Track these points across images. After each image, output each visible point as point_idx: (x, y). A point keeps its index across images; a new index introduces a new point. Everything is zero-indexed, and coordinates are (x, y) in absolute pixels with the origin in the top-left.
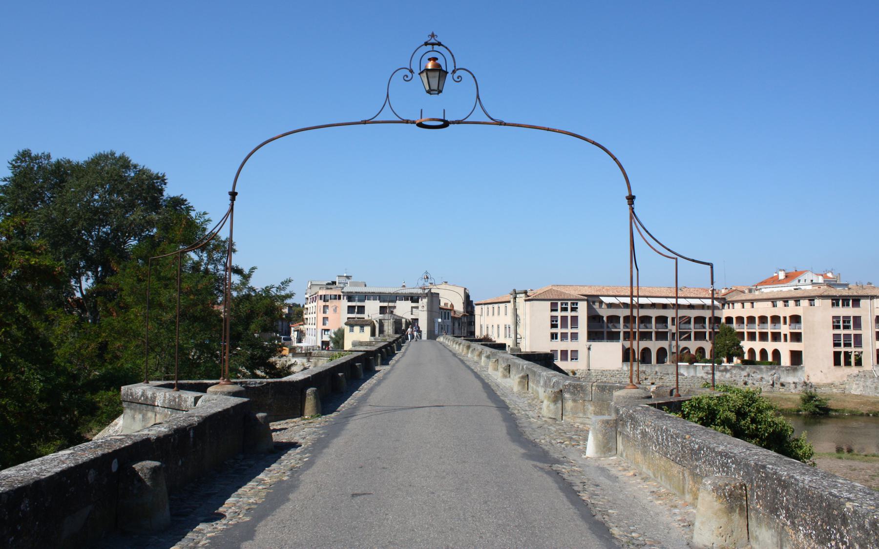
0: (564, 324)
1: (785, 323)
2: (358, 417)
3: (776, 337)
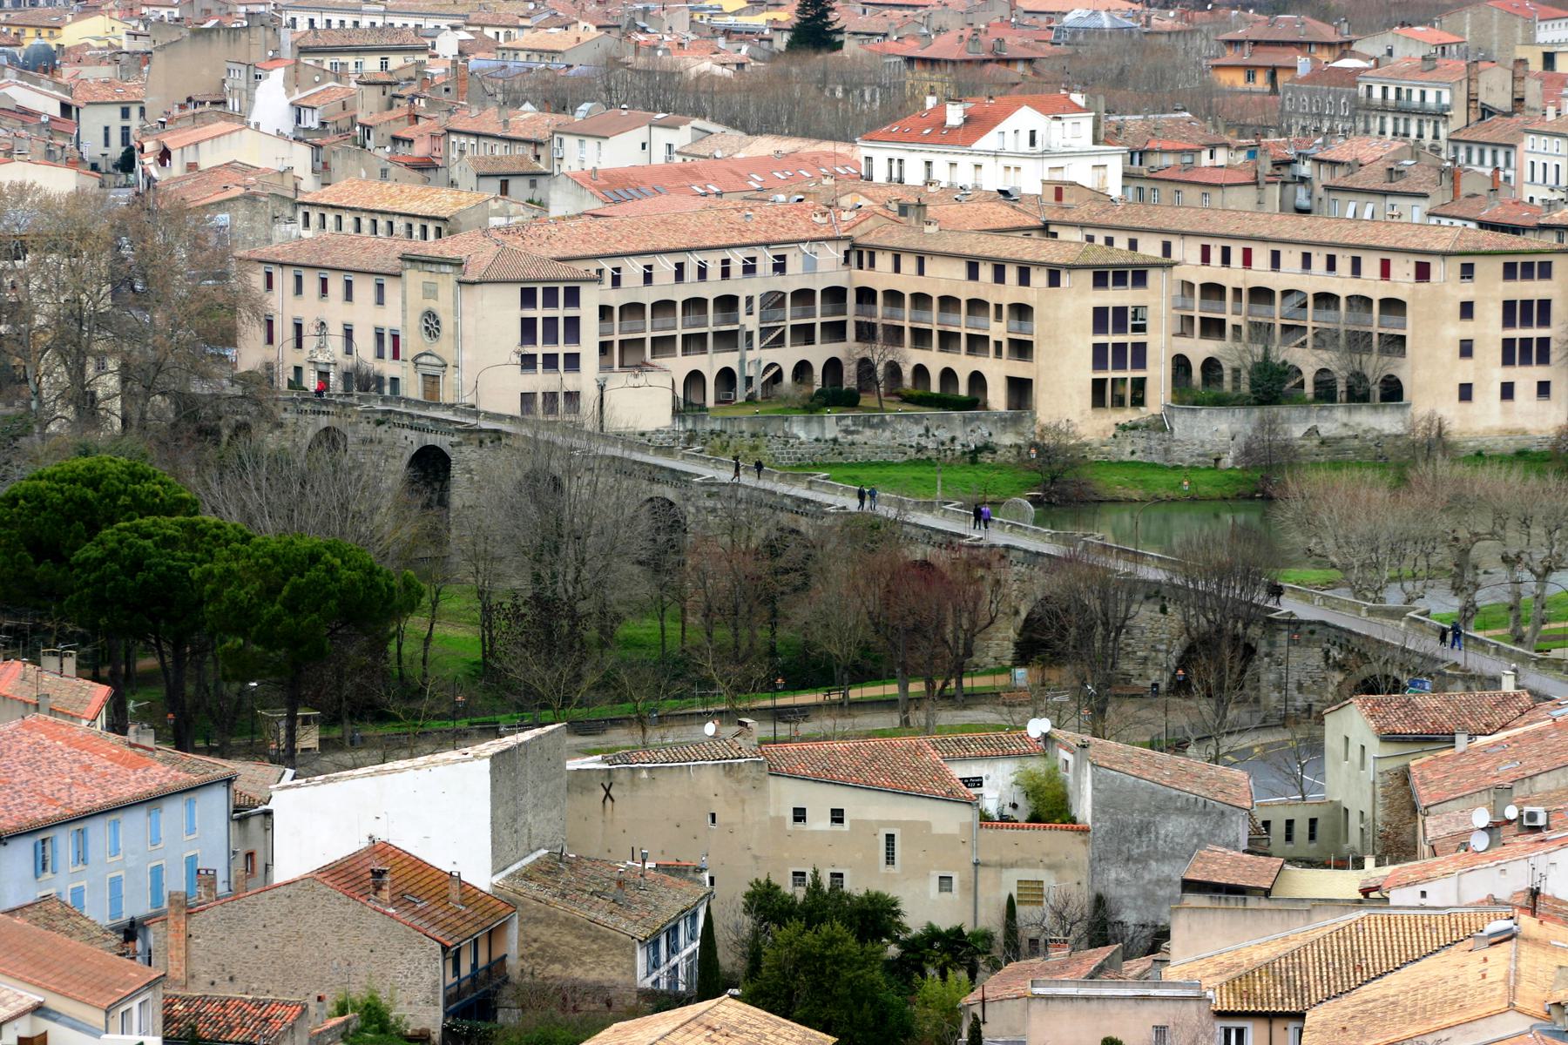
1: (999, 316)
2: (1071, 780)
3: (977, 343)
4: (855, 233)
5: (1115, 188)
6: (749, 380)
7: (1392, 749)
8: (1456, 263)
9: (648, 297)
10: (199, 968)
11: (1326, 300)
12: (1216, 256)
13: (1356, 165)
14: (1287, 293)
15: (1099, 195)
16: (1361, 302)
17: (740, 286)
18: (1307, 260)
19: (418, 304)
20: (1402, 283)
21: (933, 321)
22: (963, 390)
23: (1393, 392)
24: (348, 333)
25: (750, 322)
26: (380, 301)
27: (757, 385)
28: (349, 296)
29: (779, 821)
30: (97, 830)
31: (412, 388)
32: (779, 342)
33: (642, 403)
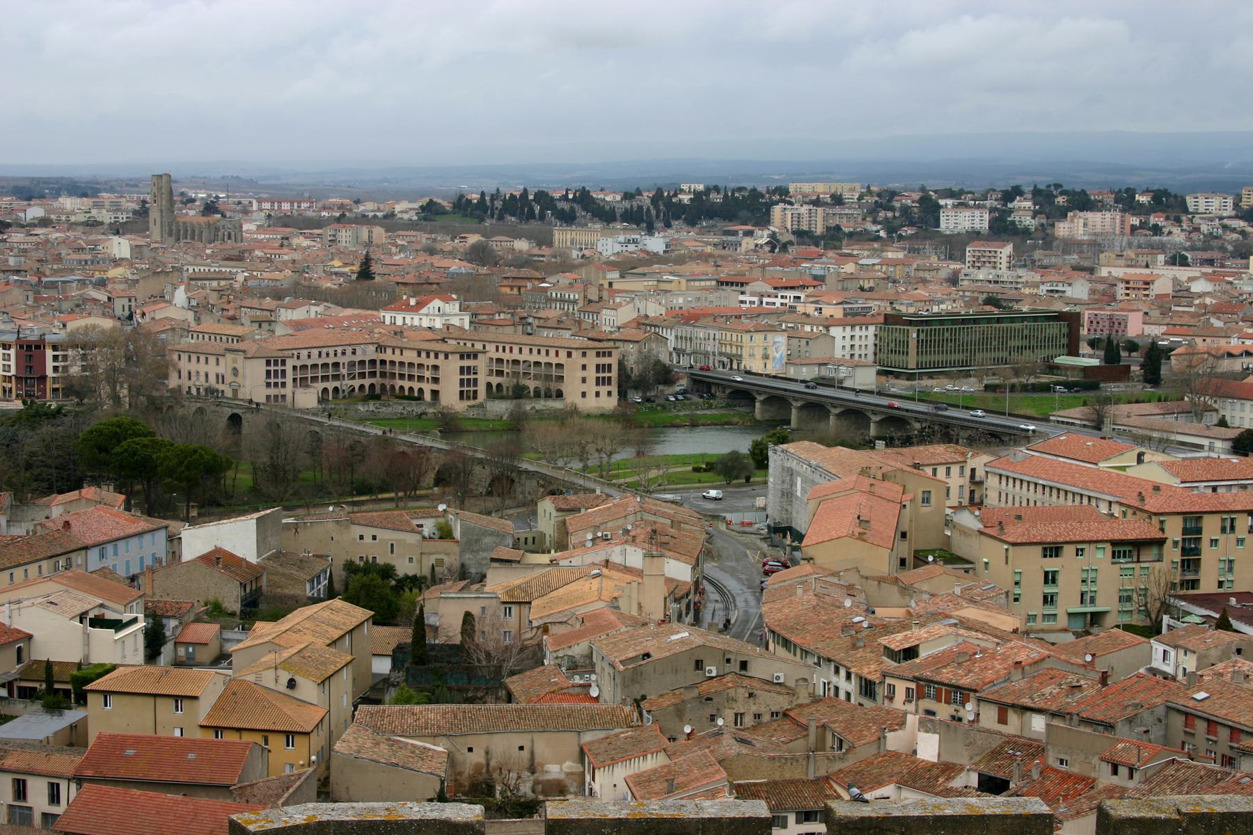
0: (276, 376)
3: (421, 378)
5: (467, 326)
9: (309, 363)
10: (157, 591)
11: (537, 364)
12: (501, 349)
13: (547, 319)
15: (461, 329)
17: (340, 359)
19: (231, 365)
20: (563, 358)
21: (406, 371)
23: (560, 394)
24: (207, 375)
25: (344, 371)
29: (354, 539)
31: (229, 394)
32: (354, 378)
33: (307, 399)
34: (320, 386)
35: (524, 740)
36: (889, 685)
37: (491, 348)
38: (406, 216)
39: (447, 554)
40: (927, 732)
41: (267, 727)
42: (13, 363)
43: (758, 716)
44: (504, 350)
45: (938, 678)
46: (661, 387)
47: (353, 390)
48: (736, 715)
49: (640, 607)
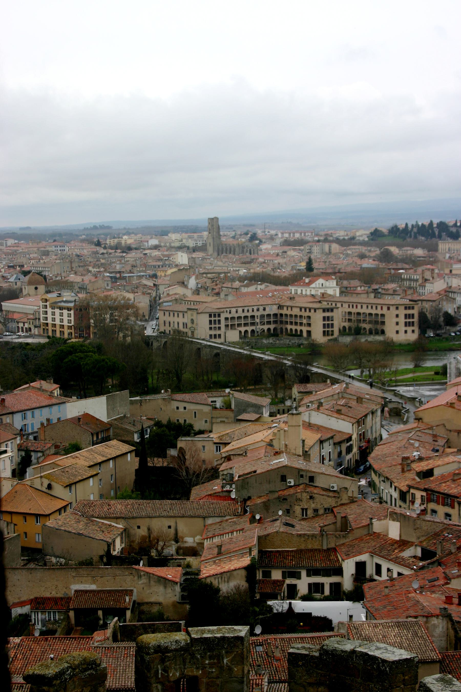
0: (215, 323)
3: (301, 324)
4: (280, 303)
5: (338, 295)
6: (258, 332)
7: (300, 395)
8: (395, 307)
9: (236, 316)
10: (47, 437)
11: (370, 314)
12: (351, 306)
13: (388, 290)
14: (363, 313)
15: (333, 296)
16: (377, 315)
17: (256, 314)
18: (367, 307)
19: (190, 318)
20: (385, 311)
21: (293, 320)
22: (299, 333)
23: (383, 332)
24: (178, 323)
25: (258, 320)
26: (184, 317)
27: (259, 333)
28: (178, 316)
29: (174, 409)
30: (37, 412)
31: (190, 334)
32: (264, 324)
33: (233, 336)
34: (243, 329)
35: (171, 522)
36: (412, 494)
37: (346, 305)
38: (361, 239)
39: (227, 418)
40: (393, 520)
41: (25, 512)
42: (72, 318)
43: (316, 510)
44: (353, 307)
45: (437, 489)
46: (448, 328)
47: (264, 331)
48: (303, 509)
49: (286, 445)
